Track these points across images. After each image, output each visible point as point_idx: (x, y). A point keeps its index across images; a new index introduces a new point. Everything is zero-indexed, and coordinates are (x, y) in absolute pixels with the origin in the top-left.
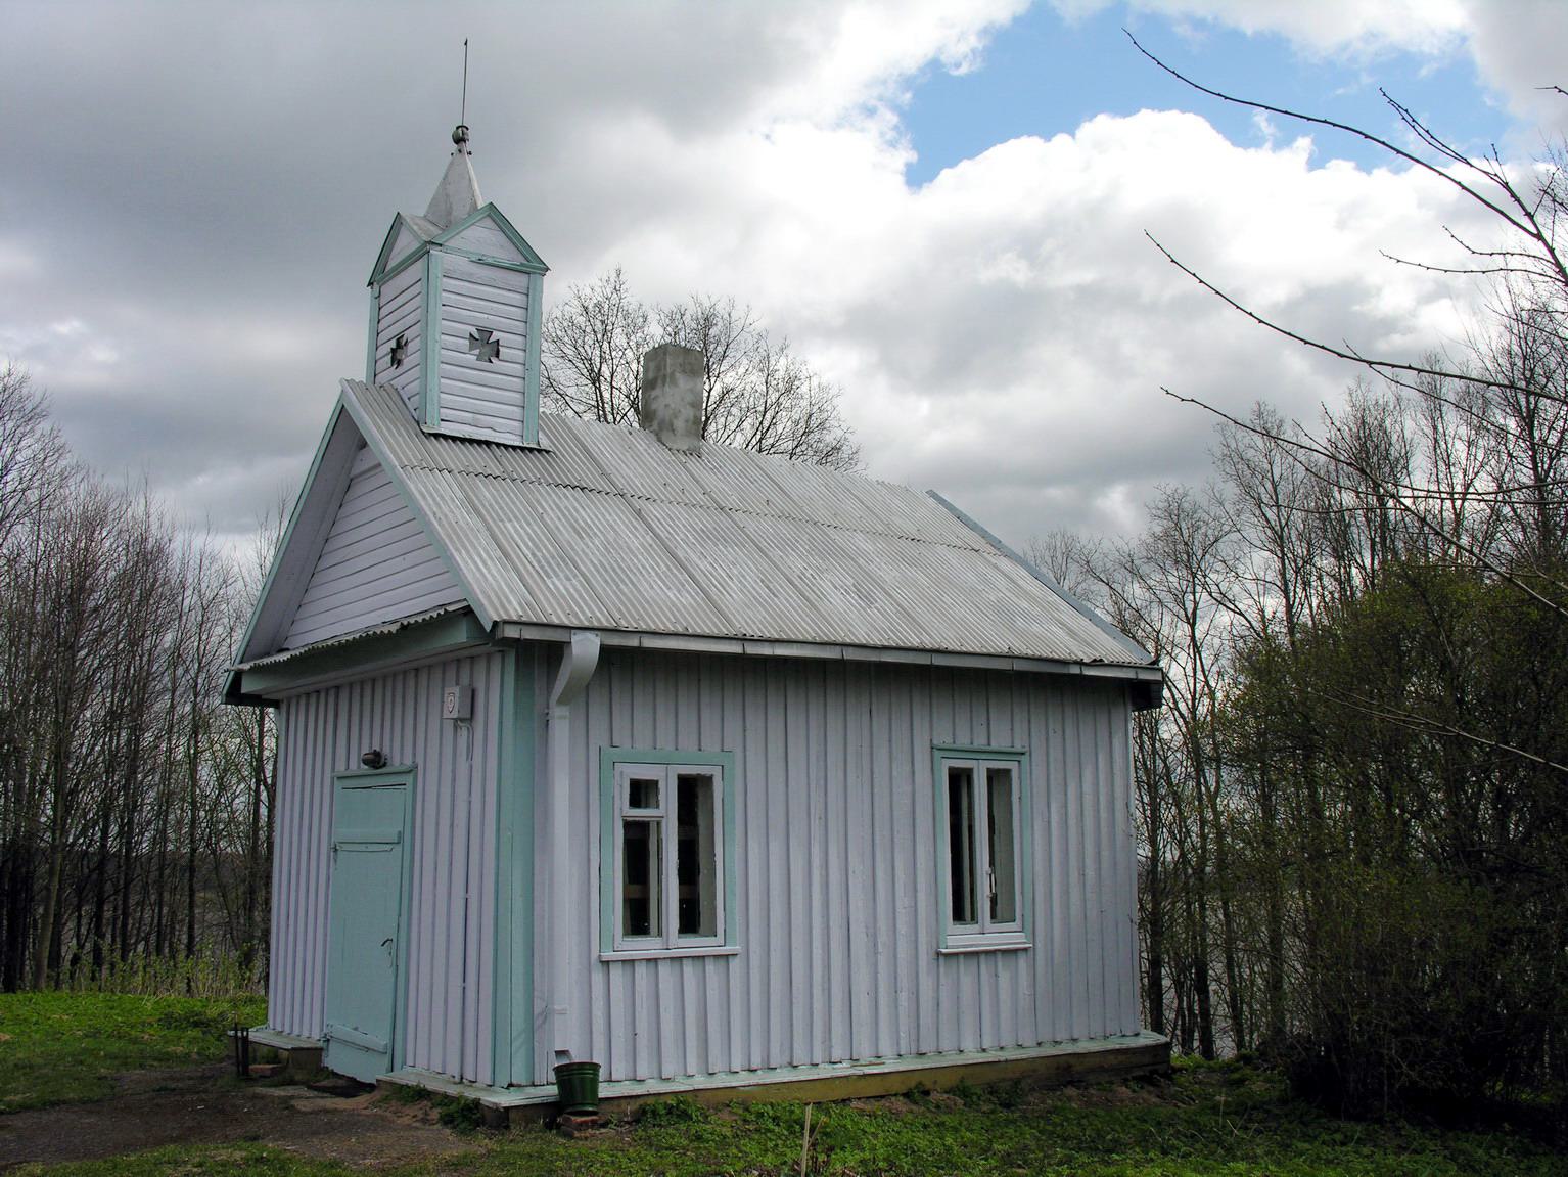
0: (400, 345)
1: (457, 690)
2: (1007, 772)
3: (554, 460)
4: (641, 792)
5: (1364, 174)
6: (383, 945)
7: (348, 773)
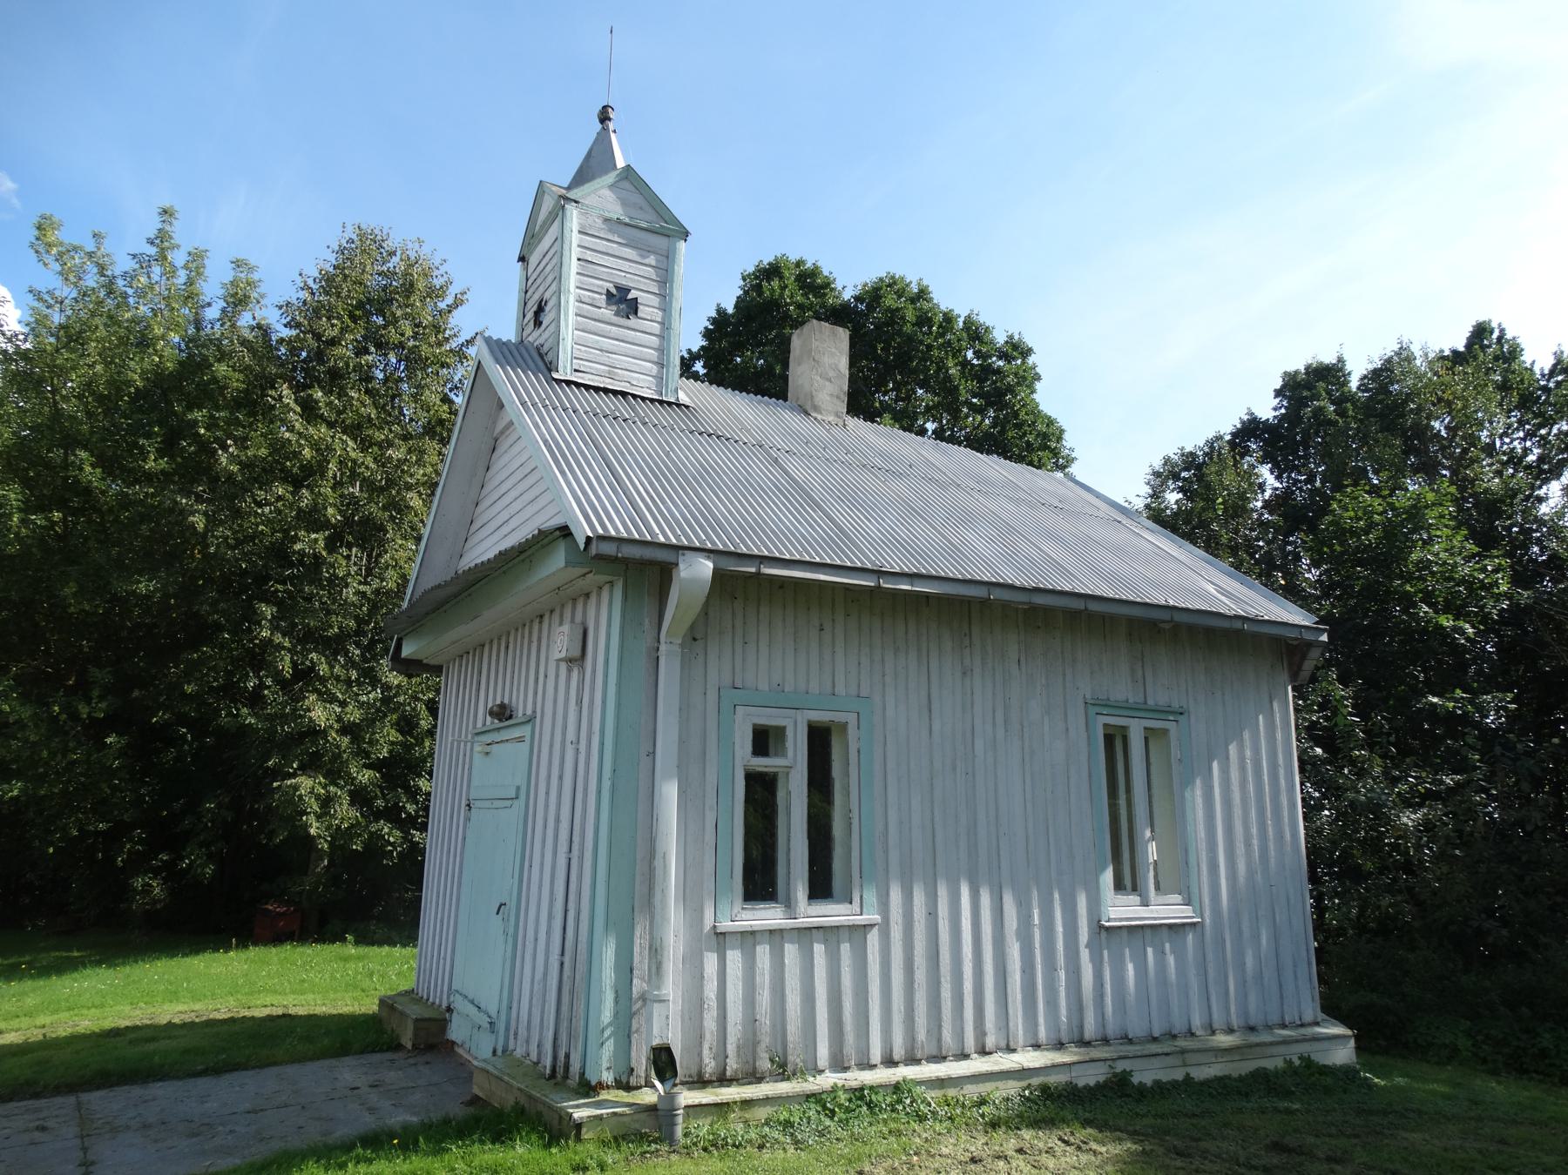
0: (540, 309)
1: (566, 628)
2: (1165, 732)
3: (693, 415)
4: (764, 740)
5: (1278, 384)
6: (498, 913)
7: (485, 729)
